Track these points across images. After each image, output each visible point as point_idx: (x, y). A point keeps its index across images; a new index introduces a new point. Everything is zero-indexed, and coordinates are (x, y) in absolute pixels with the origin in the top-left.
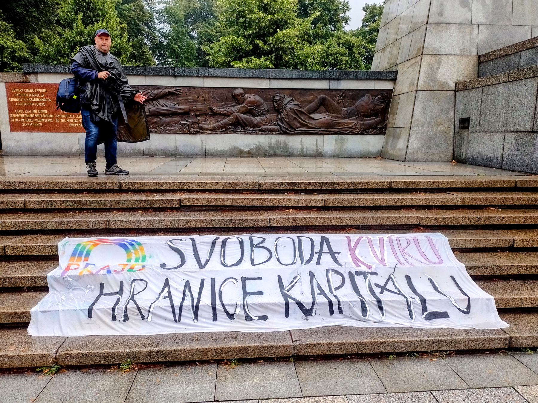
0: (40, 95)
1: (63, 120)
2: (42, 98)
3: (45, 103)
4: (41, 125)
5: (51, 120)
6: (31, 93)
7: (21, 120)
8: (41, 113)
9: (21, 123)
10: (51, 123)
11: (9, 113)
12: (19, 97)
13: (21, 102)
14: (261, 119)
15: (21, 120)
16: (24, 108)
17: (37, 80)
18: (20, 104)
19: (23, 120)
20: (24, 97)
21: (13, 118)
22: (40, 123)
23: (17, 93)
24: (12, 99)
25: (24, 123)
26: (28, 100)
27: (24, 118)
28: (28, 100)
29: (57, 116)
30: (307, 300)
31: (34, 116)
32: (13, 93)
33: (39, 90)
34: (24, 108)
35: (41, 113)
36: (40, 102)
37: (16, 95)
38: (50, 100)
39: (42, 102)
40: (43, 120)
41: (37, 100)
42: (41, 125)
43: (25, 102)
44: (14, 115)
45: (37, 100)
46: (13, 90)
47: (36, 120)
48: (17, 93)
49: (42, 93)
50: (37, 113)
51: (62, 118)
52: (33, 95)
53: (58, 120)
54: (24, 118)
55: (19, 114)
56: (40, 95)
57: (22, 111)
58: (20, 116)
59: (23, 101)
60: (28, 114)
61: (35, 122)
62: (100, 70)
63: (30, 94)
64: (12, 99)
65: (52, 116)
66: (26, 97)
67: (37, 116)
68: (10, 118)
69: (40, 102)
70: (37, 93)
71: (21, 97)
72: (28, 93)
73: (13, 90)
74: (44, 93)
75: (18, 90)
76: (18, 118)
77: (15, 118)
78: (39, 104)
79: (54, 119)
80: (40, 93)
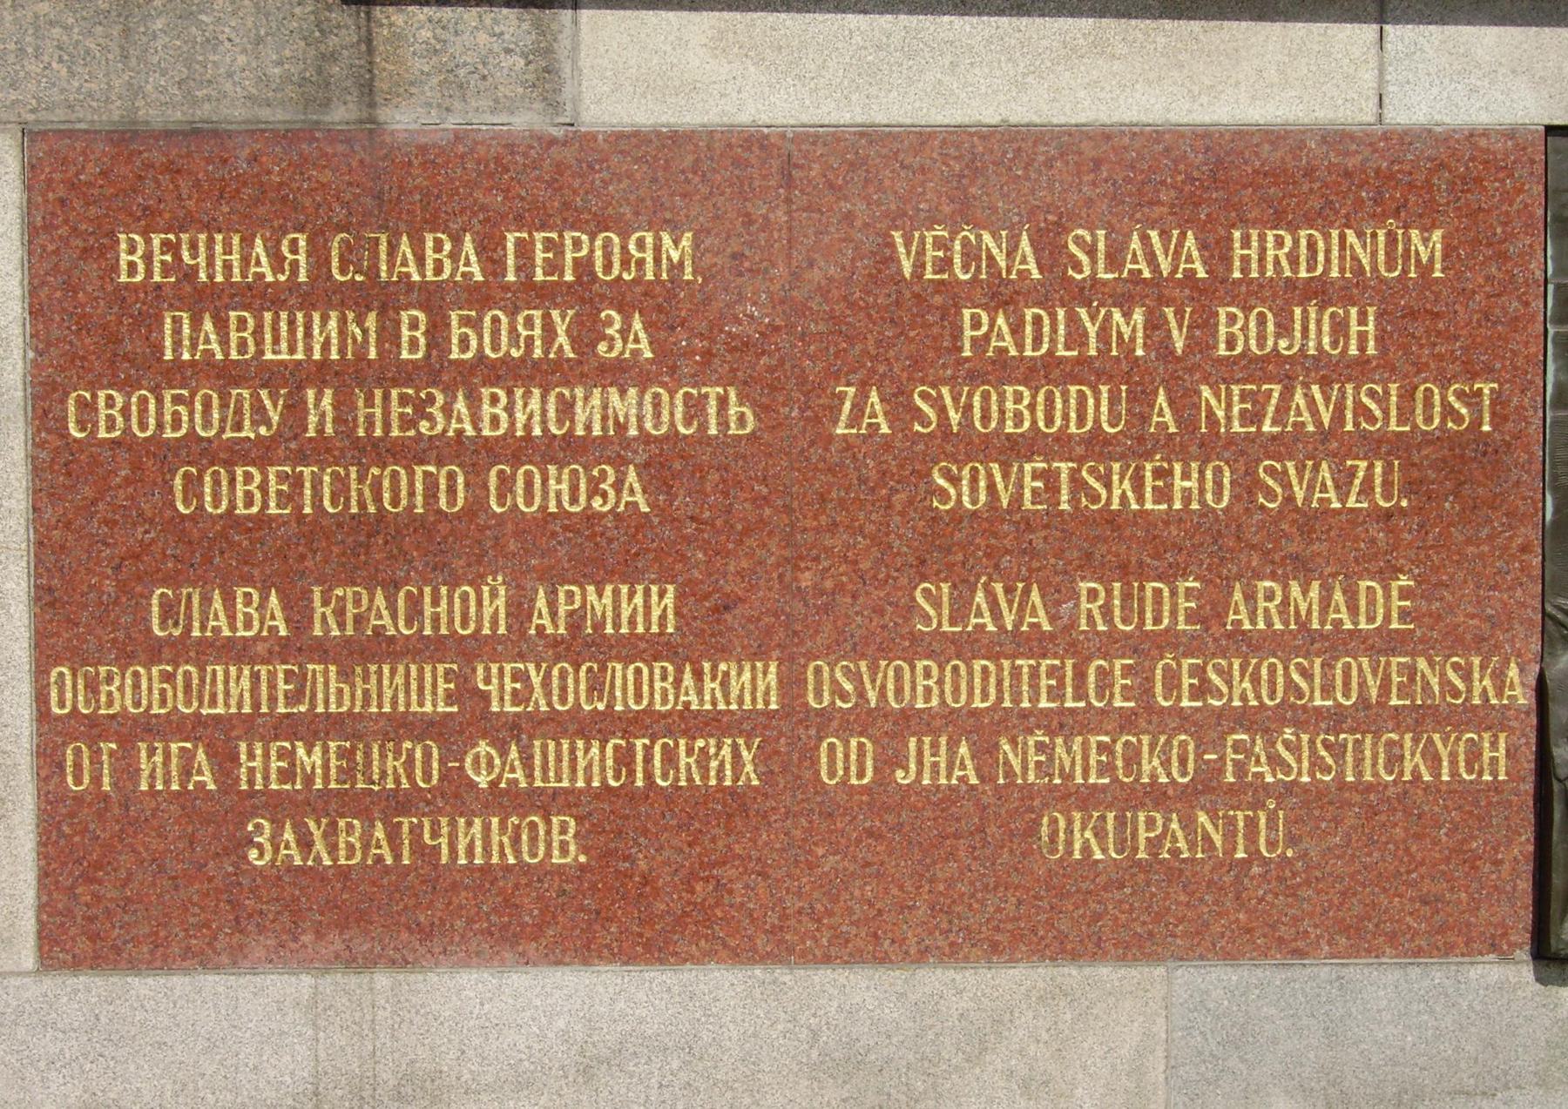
0: (587, 333)
1: (155, 767)
2: (617, 374)
3: (665, 462)
4: (561, 844)
5: (732, 764)
6: (434, 299)
7: (225, 761)
8: (583, 644)
9: (235, 808)
10: (735, 803)
11: (45, 654)
12: (226, 375)
13: (261, 454)
14: (478, 774)
15: (225, 761)
16: (290, 555)
17: (546, 75)
18: (250, 492)
19: (258, 765)
20: (321, 373)
21: (94, 728)
22: (547, 802)
23: (207, 300)
24: (113, 413)
25: (278, 807)
26: (380, 414)
27: (289, 728)
28: (380, 414)
29: (831, 682)
30: (776, 338)
31: (465, 692)
32: (144, 307)
33: (576, 246)
34: (290, 555)
35: (583, 644)
36: (568, 449)
37: (182, 337)
38: (741, 418)
39: (612, 447)
40: (593, 764)
41: (531, 411)
42: (561, 844)
43: (320, 452)
44: (131, 691)
45: (531, 411)
46: (137, 257)
47: (484, 765)
48: (207, 300)
49: (625, 298)
50: (518, 641)
51: (908, 721)
52: (467, 341)
53: (844, 762)
54: (289, 728)
55: (227, 654)
56: (587, 333)
57: (257, 613)
58: (233, 690)
59: (288, 444)
60: (364, 650)
61: (455, 795)
62: (1345, 592)
63: (412, 326)
64: (113, 413)
65: (752, 684)
66: (347, 376)
67: (497, 684)
68: (54, 735)
69: (568, 449)
70: (544, 295)
71: (270, 376)
72: (383, 299)
73: (137, 257)
74: (656, 301)
75: (219, 258)
76: (194, 727)
77: (135, 730)
78: (557, 489)
79: (787, 733)
80: (586, 294)
